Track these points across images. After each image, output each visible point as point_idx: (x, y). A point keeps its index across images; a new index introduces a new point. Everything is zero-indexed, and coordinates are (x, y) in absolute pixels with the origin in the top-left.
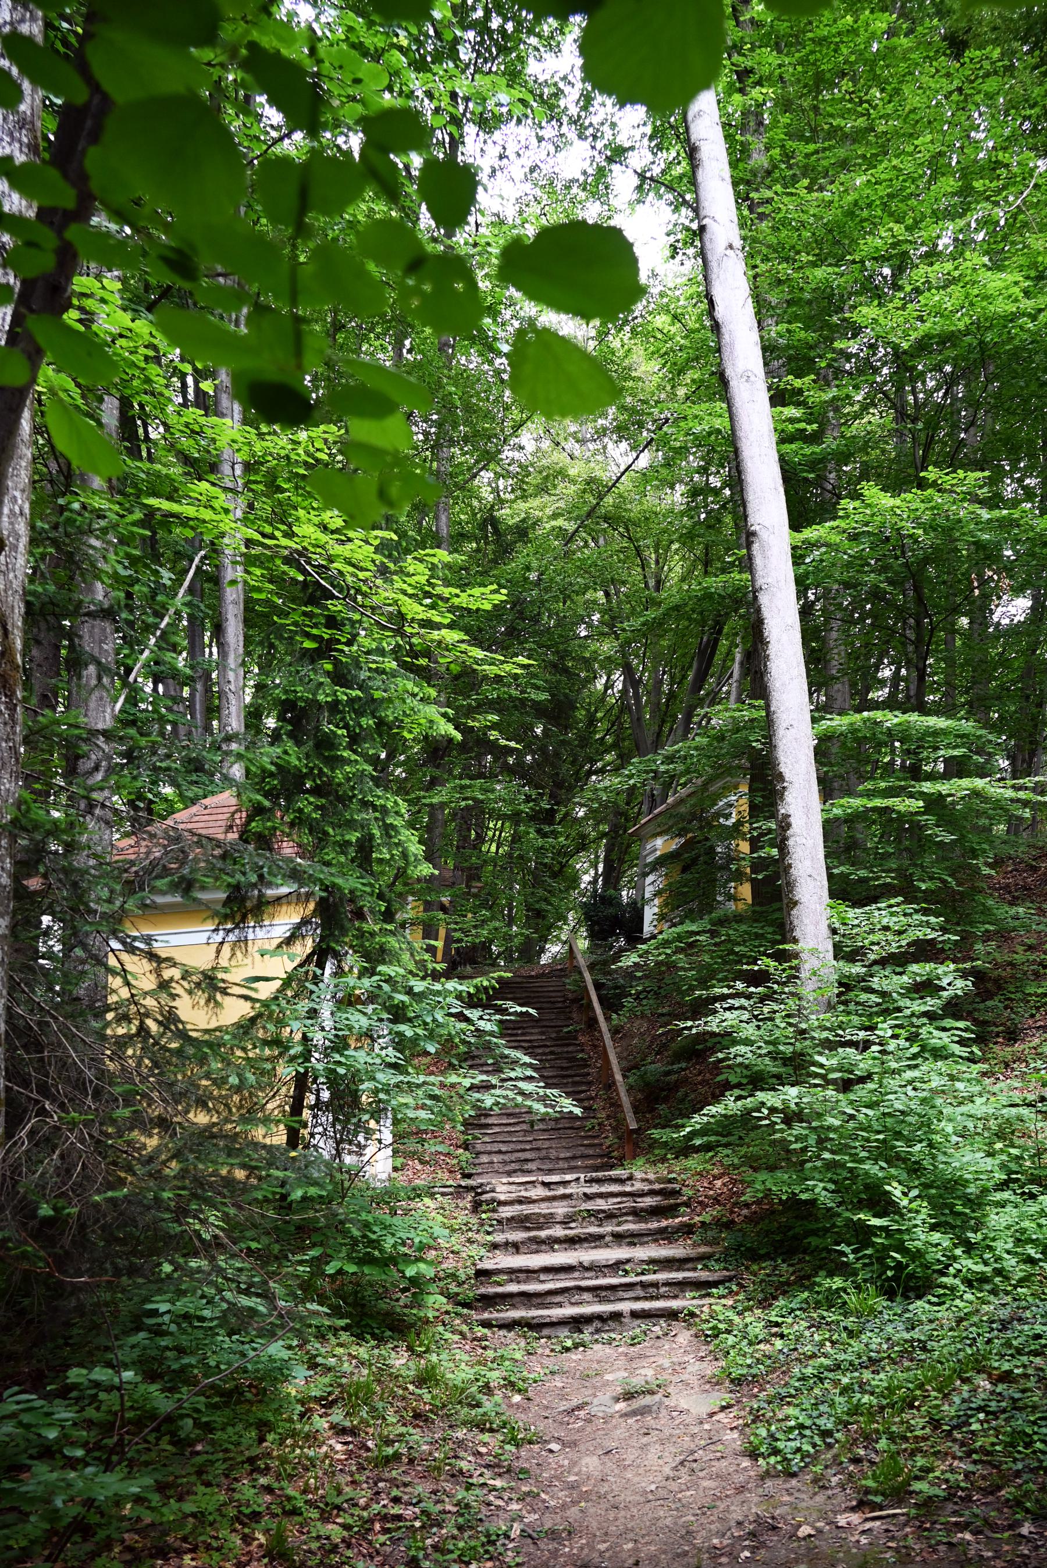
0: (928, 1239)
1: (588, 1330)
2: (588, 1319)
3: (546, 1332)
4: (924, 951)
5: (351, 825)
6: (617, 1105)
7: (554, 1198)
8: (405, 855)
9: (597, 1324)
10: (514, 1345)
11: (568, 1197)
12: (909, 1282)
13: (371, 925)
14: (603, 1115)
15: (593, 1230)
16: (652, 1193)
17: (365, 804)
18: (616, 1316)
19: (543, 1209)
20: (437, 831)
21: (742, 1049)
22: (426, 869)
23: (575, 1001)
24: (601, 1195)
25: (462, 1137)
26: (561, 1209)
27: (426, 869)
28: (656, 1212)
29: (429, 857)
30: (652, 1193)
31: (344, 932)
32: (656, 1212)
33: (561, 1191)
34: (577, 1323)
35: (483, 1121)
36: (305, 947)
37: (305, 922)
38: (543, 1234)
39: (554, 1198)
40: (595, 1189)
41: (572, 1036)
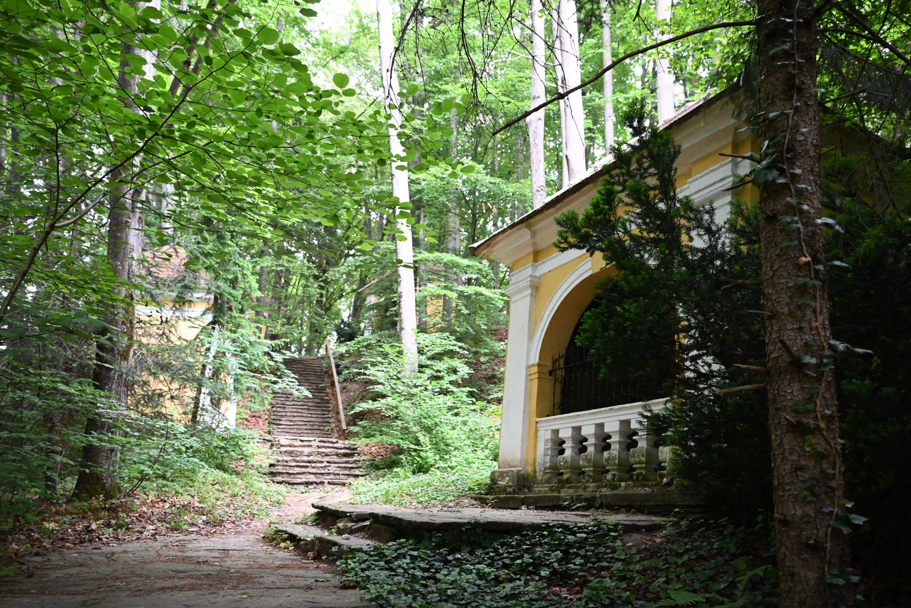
0: (430, 456)
1: (310, 487)
2: (312, 483)
3: (295, 486)
4: (451, 354)
5: (227, 271)
6: (340, 421)
7: (304, 446)
8: (250, 287)
9: (315, 485)
10: (282, 488)
11: (310, 446)
12: (422, 469)
13: (235, 313)
14: (333, 425)
15: (320, 459)
16: (345, 448)
17: (235, 264)
18: (322, 483)
19: (300, 449)
20: (264, 277)
21: (380, 387)
22: (259, 294)
23: (326, 372)
24: (324, 447)
25: (268, 429)
26: (307, 450)
27: (259, 294)
28: (345, 455)
29: (260, 289)
30: (345, 448)
31: (224, 315)
32: (345, 455)
33: (307, 443)
34: (307, 484)
35: (278, 422)
36: (209, 317)
37: (208, 309)
38: (298, 459)
39: (304, 446)
40: (323, 444)
41: (324, 389)
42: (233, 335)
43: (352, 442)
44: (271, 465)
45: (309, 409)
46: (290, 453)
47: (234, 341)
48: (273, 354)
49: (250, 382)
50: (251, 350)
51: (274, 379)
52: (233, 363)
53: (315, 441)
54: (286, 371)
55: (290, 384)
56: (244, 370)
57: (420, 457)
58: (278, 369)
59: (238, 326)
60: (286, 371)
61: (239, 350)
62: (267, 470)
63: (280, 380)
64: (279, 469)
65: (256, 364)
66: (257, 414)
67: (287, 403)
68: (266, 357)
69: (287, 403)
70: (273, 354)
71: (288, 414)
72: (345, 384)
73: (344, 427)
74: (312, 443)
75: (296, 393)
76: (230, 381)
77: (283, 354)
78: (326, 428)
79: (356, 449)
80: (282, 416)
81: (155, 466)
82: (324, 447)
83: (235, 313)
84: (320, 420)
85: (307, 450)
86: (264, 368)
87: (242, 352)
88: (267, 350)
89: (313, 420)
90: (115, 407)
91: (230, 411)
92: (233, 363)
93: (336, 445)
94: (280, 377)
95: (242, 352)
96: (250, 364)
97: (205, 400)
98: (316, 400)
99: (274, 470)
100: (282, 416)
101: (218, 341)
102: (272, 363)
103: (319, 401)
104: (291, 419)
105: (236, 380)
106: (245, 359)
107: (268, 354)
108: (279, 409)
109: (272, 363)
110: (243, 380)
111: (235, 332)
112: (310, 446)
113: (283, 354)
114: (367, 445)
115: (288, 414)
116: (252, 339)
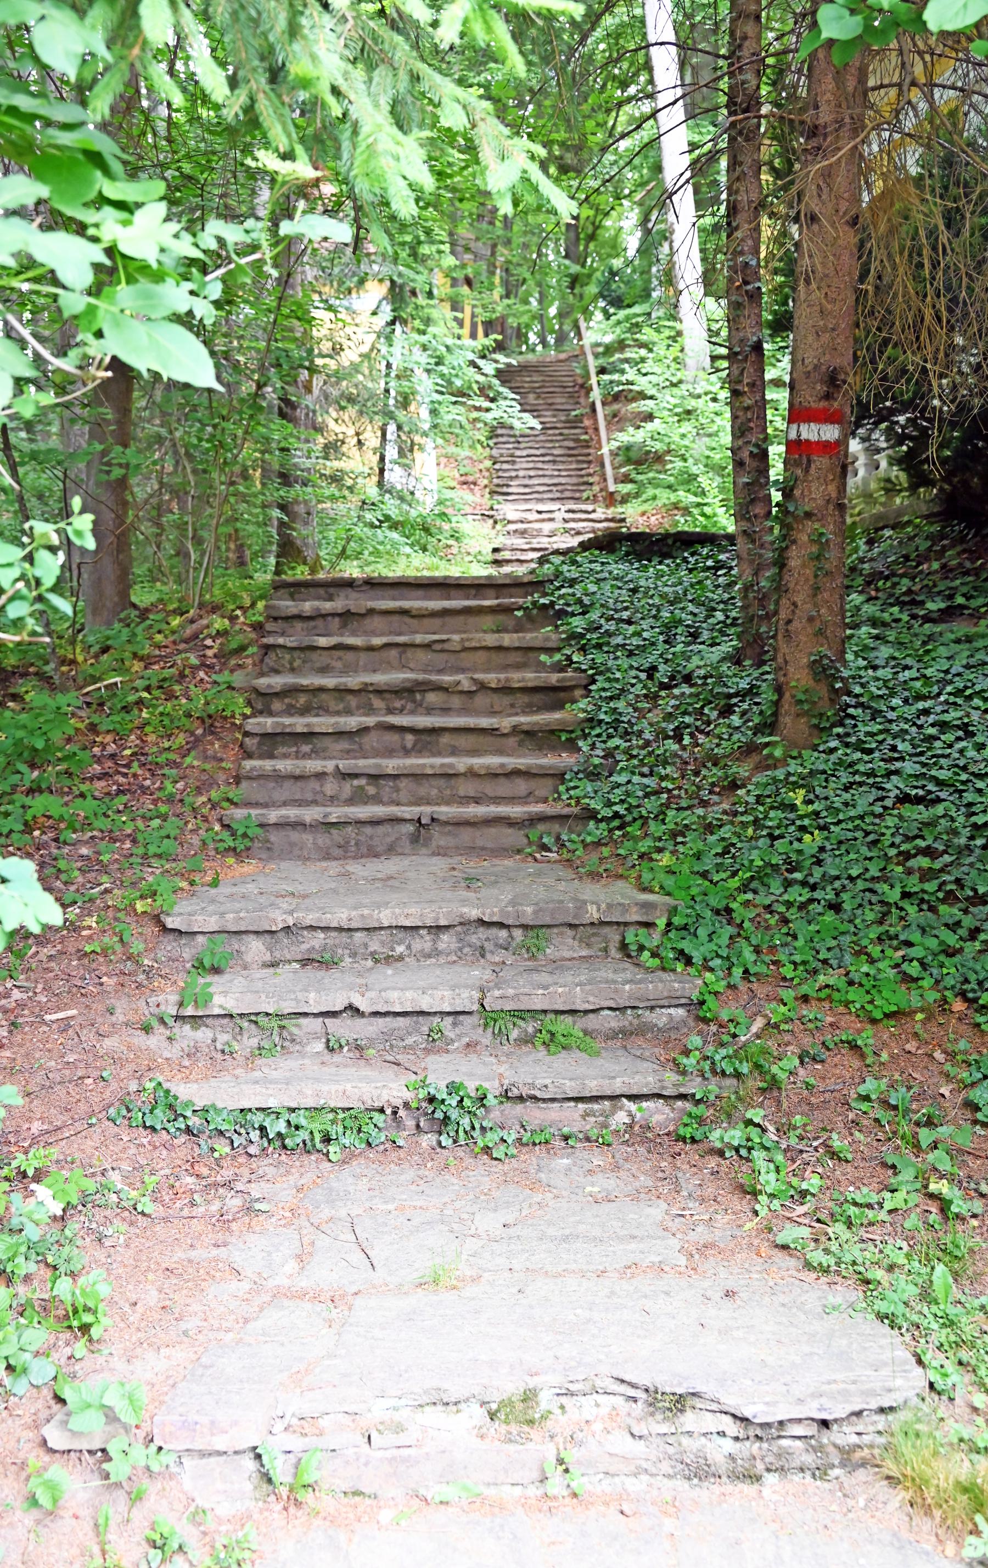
13: (421, 300)
16: (607, 520)
23: (582, 386)
24: (574, 520)
25: (489, 503)
30: (607, 520)
31: (407, 305)
35: (505, 490)
36: (386, 313)
40: (571, 515)
41: (579, 419)
42: (423, 339)
43: (620, 510)
44: (496, 550)
45: (554, 462)
46: (523, 533)
47: (425, 348)
48: (481, 363)
49: (452, 413)
50: (449, 359)
51: (486, 404)
52: (424, 385)
53: (560, 510)
54: (501, 389)
55: (508, 409)
56: (442, 393)
57: (703, 515)
58: (490, 387)
59: (428, 321)
60: (501, 389)
61: (433, 361)
62: (490, 557)
63: (493, 405)
64: (506, 555)
65: (458, 383)
66: (470, 479)
67: (518, 453)
68: (472, 370)
69: (518, 453)
70: (481, 363)
71: (521, 473)
72: (616, 407)
73: (612, 488)
74: (558, 515)
75: (517, 424)
76: (424, 413)
77: (496, 361)
78: (585, 495)
79: (623, 520)
80: (511, 478)
81: (188, 760)
82: (574, 520)
83: (421, 300)
84: (575, 480)
85: (547, 527)
86: (470, 388)
87: (437, 364)
88: (471, 356)
89: (563, 480)
90: (305, 457)
91: (427, 462)
92: (424, 385)
93: (592, 516)
94: (493, 400)
95: (437, 364)
96: (450, 383)
97: (391, 452)
98: (567, 443)
99: (499, 556)
100: (511, 478)
101: (404, 350)
102: (481, 379)
103: (571, 444)
104: (526, 482)
105: (434, 412)
106: (442, 376)
107: (473, 364)
108: (505, 466)
109: (481, 379)
110: (442, 410)
111: (424, 333)
112: (552, 520)
113: (496, 361)
114: (643, 514)
115: (521, 473)
116: (450, 341)
